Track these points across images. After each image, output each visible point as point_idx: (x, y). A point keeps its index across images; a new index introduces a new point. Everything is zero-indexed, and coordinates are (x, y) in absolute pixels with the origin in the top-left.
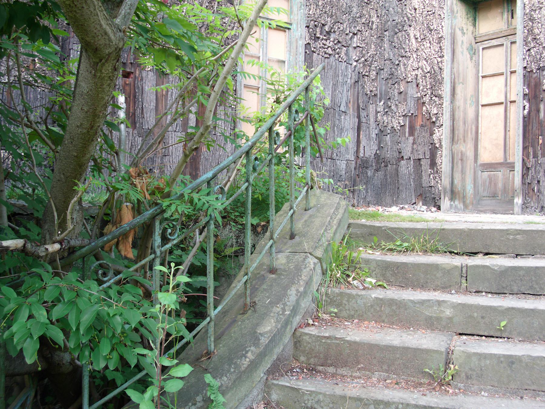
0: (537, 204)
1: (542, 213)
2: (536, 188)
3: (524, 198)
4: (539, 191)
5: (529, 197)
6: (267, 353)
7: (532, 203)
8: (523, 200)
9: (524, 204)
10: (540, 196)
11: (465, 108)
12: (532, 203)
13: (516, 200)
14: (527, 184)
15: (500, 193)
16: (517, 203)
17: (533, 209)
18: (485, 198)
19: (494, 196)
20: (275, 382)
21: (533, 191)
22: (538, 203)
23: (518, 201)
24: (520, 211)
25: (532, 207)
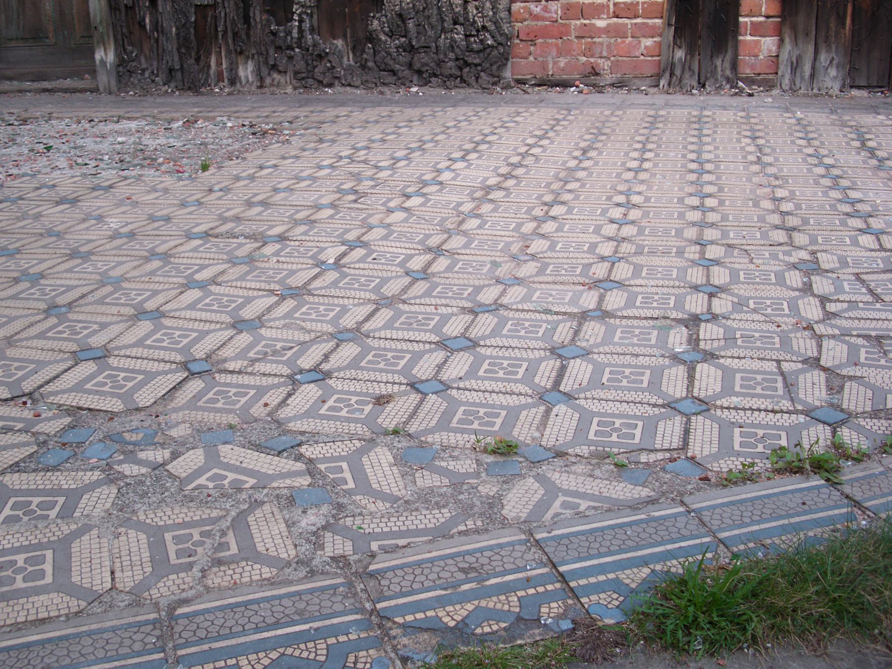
0: (155, 64)
1: (173, 85)
2: (147, 21)
3: (121, 50)
4: (156, 26)
5: (132, 44)
6: (285, 454)
7: (143, 60)
8: (118, 55)
9: (121, 63)
10: (162, 39)
11: (192, 600)
12: (143, 60)
13: (99, 55)
14: (123, 10)
15: (51, 28)
16: (103, 62)
17: (147, 74)
18: (13, 44)
19: (36, 35)
20: (845, 510)
21: (142, 26)
22: (160, 59)
23: (106, 56)
24: (113, 83)
25: (144, 70)
